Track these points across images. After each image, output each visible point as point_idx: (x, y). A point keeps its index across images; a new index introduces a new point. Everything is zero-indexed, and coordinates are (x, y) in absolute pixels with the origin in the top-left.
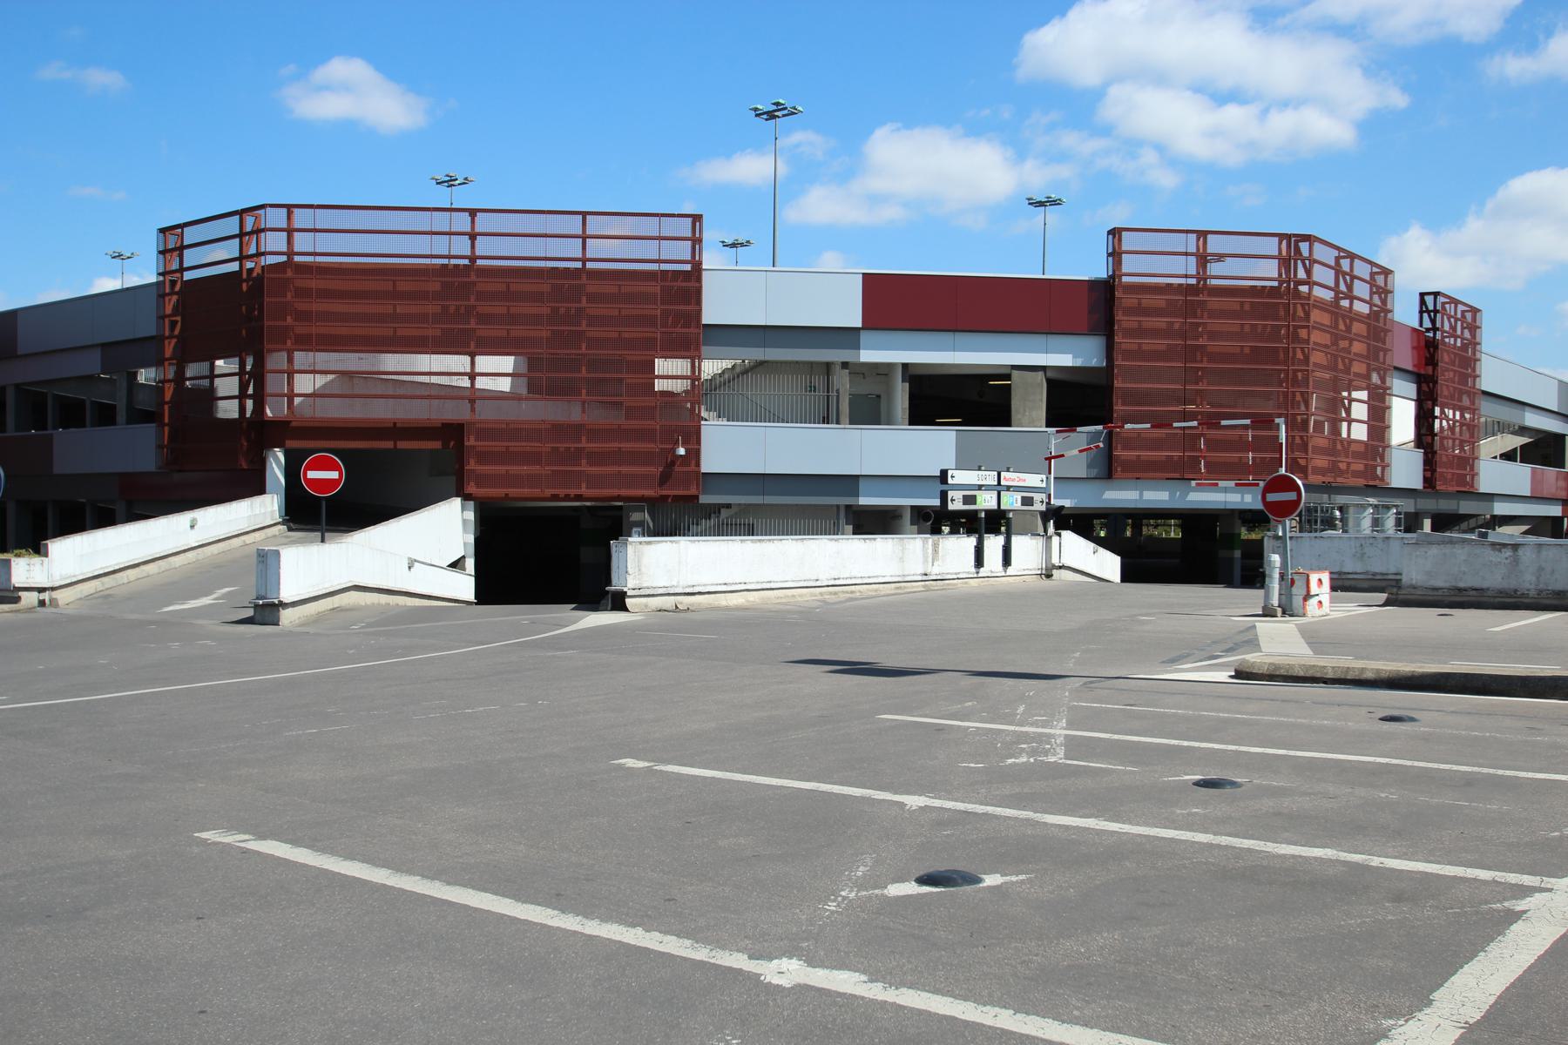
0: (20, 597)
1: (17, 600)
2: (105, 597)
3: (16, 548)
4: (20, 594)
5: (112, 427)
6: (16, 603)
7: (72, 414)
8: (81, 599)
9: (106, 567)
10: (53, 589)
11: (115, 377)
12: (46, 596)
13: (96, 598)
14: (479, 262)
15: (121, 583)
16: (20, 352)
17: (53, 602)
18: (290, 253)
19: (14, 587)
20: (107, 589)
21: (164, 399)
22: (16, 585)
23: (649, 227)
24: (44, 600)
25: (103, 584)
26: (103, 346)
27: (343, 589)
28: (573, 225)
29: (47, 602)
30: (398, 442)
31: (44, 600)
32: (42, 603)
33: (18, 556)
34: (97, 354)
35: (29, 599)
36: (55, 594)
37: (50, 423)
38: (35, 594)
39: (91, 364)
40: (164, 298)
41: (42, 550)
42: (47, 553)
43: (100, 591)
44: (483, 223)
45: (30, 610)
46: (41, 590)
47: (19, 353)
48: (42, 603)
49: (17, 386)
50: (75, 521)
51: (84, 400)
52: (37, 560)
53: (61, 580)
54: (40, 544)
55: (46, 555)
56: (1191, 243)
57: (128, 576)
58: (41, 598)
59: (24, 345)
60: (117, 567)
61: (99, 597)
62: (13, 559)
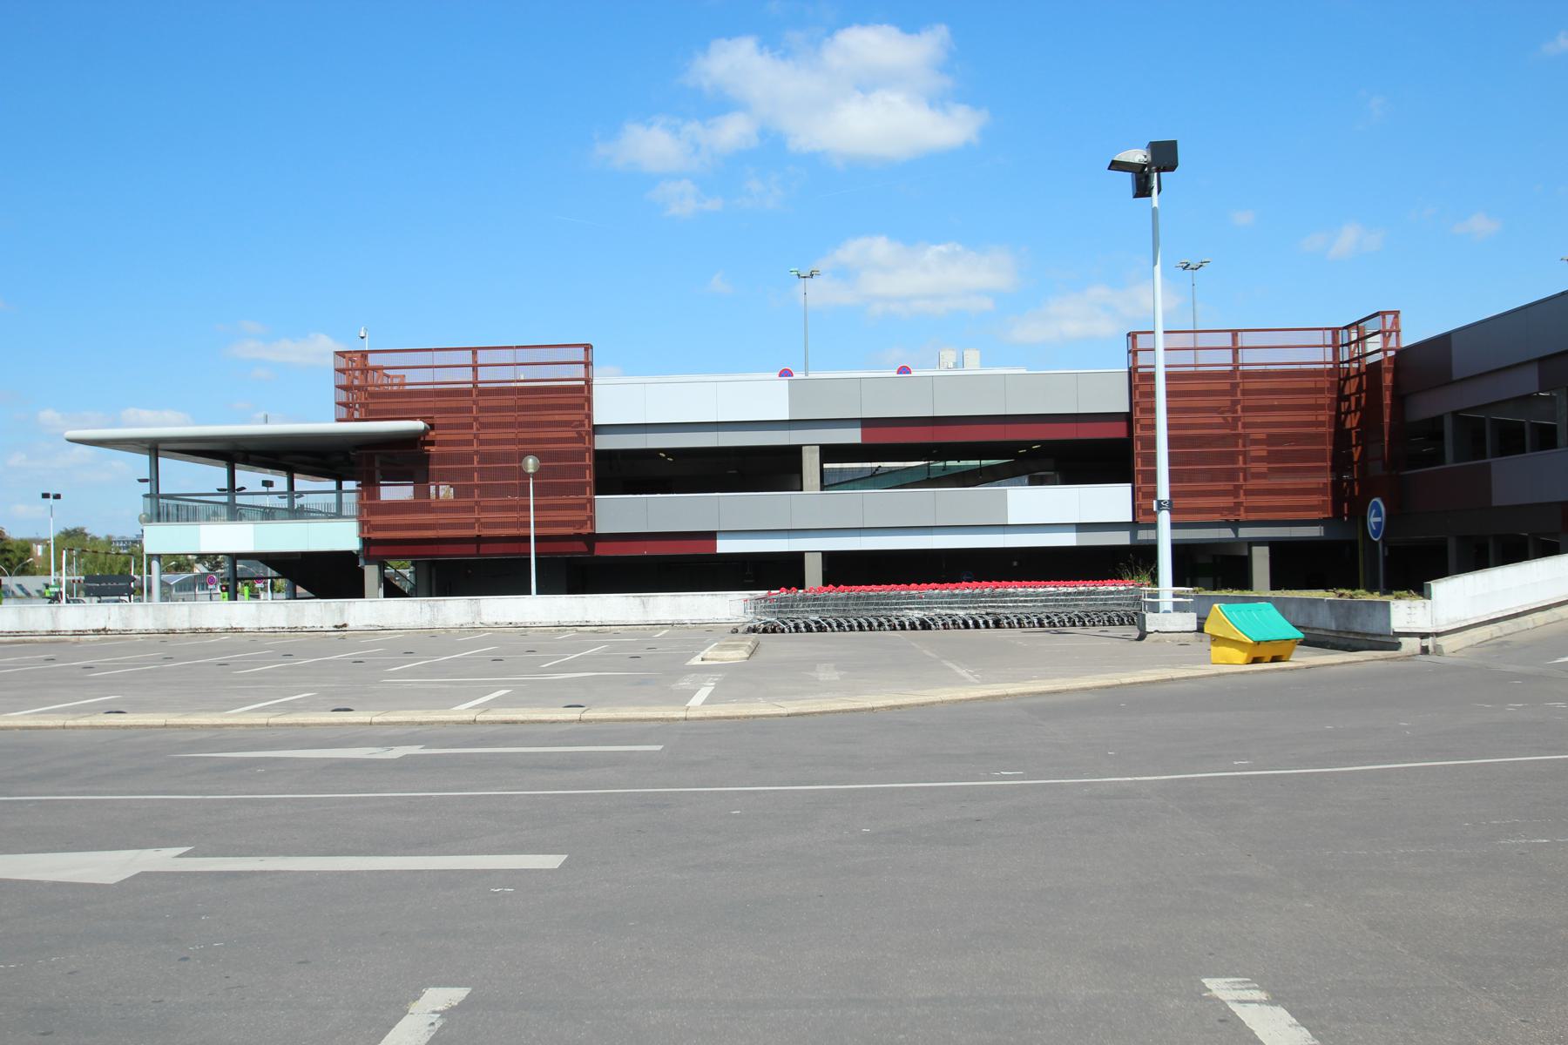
0: (1400, 644)
1: (1397, 646)
2: (1500, 645)
3: (1396, 590)
4: (1401, 639)
5: (1554, 450)
6: (1396, 650)
7: (1512, 440)
8: (1472, 646)
9: (1506, 610)
10: (1438, 634)
11: (1554, 395)
12: (1429, 642)
13: (1489, 645)
14: (480, 385)
15: (1525, 627)
16: (1456, 376)
17: (1438, 650)
18: (475, 383)
19: (1394, 632)
20: (1506, 635)
21: (297, 472)
22: (1396, 630)
23: (507, 357)
24: (1427, 647)
25: (1501, 629)
26: (1541, 360)
27: (1509, 616)
28: (467, 358)
29: (1431, 649)
30: (344, 483)
31: (1427, 647)
32: (1425, 650)
33: (1398, 598)
34: (1534, 369)
35: (1410, 645)
36: (1440, 641)
37: (1488, 451)
38: (1417, 640)
39: (1528, 382)
40: (1384, 318)
41: (1426, 593)
42: (1430, 594)
43: (1497, 637)
44: (483, 357)
45: (1409, 657)
46: (1424, 636)
47: (1454, 378)
48: (1425, 650)
49: (1455, 413)
50: (1479, 557)
51: (1523, 422)
52: (1418, 603)
53: (1447, 624)
54: (1423, 585)
55: (1429, 598)
56: (467, 358)
57: (1533, 620)
58: (1424, 645)
59: (1461, 365)
60: (1520, 610)
61: (1493, 644)
62: (1392, 602)
